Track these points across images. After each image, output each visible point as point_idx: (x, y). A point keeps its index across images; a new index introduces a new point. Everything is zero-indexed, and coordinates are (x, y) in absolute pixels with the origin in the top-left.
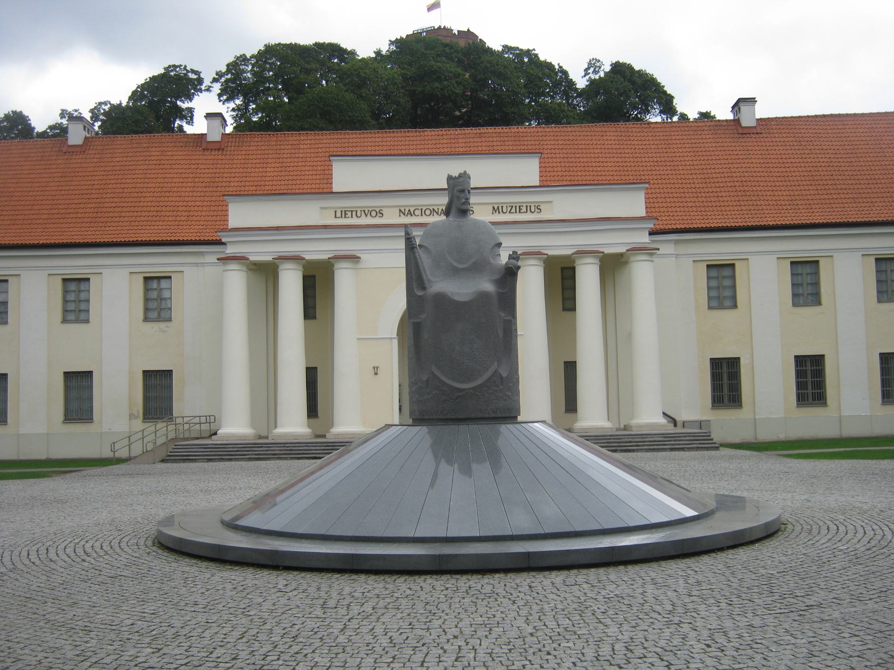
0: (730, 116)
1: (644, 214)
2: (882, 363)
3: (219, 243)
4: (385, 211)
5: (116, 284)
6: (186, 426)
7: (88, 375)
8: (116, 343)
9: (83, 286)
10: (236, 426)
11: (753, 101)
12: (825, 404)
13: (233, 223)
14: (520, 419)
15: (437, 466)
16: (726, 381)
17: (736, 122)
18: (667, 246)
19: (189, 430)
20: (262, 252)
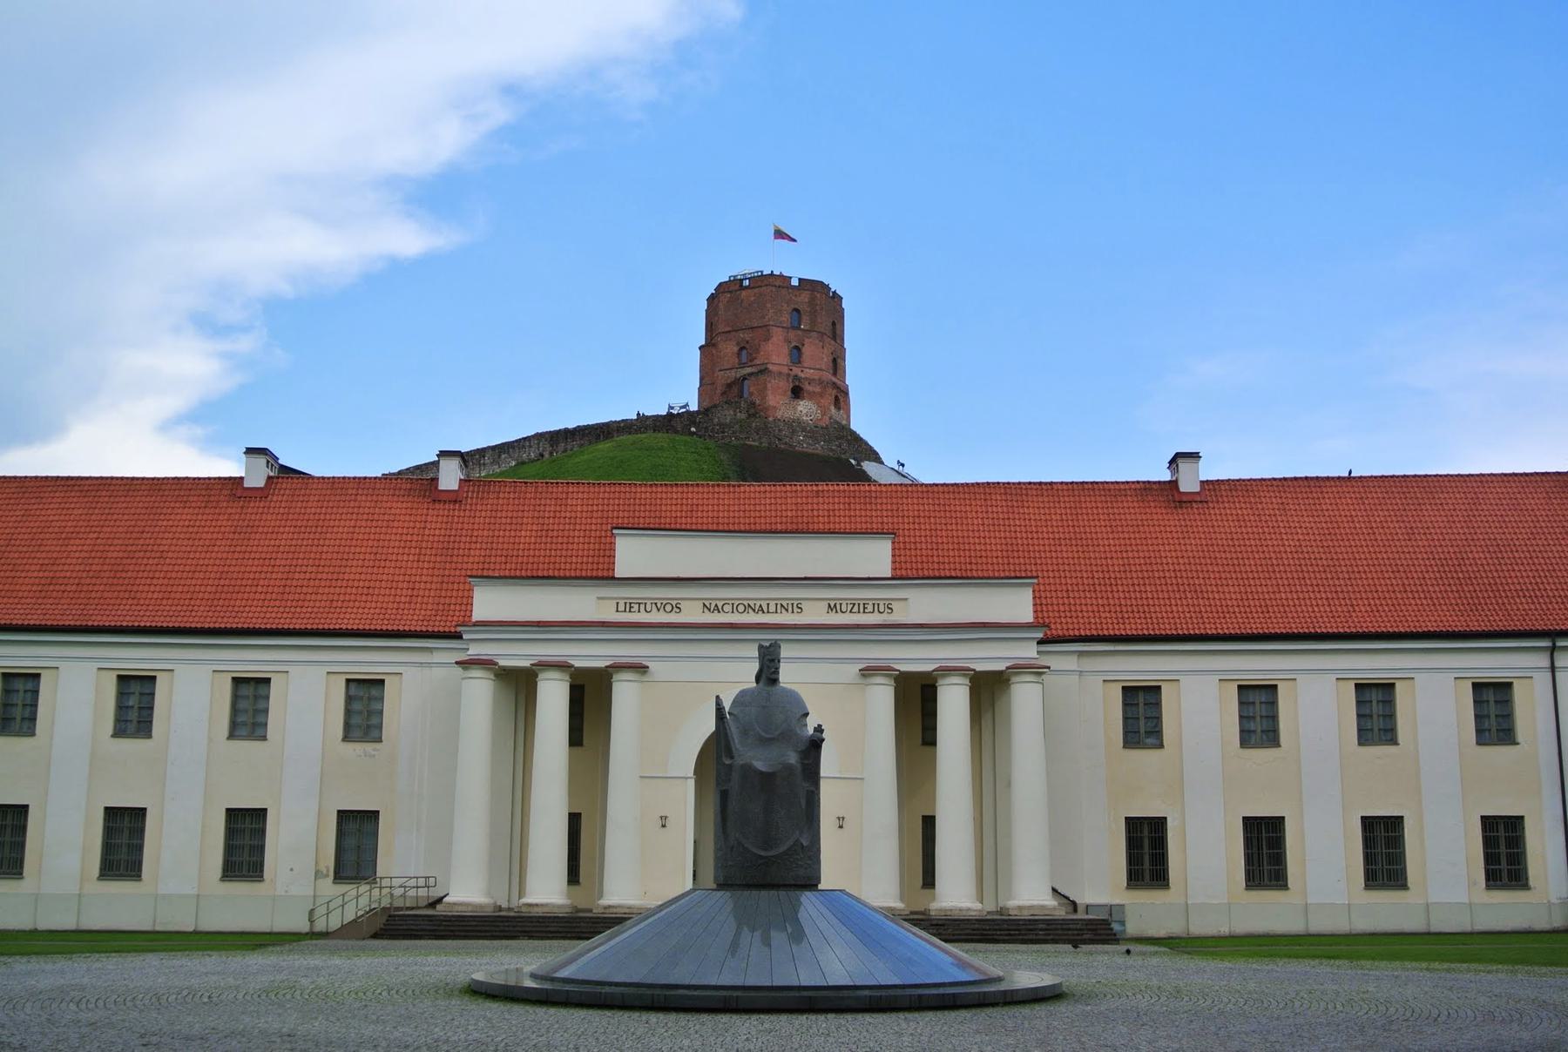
0: (1166, 476)
1: (1031, 619)
2: (1484, 829)
3: (458, 636)
4: (683, 605)
5: (307, 685)
6: (398, 892)
7: (259, 815)
8: (301, 771)
9: (262, 690)
10: (468, 890)
11: (1194, 456)
12: (1285, 887)
13: (478, 614)
14: (820, 887)
15: (738, 934)
16: (1147, 848)
17: (1173, 484)
18: (1063, 661)
19: (404, 896)
20: (516, 655)
